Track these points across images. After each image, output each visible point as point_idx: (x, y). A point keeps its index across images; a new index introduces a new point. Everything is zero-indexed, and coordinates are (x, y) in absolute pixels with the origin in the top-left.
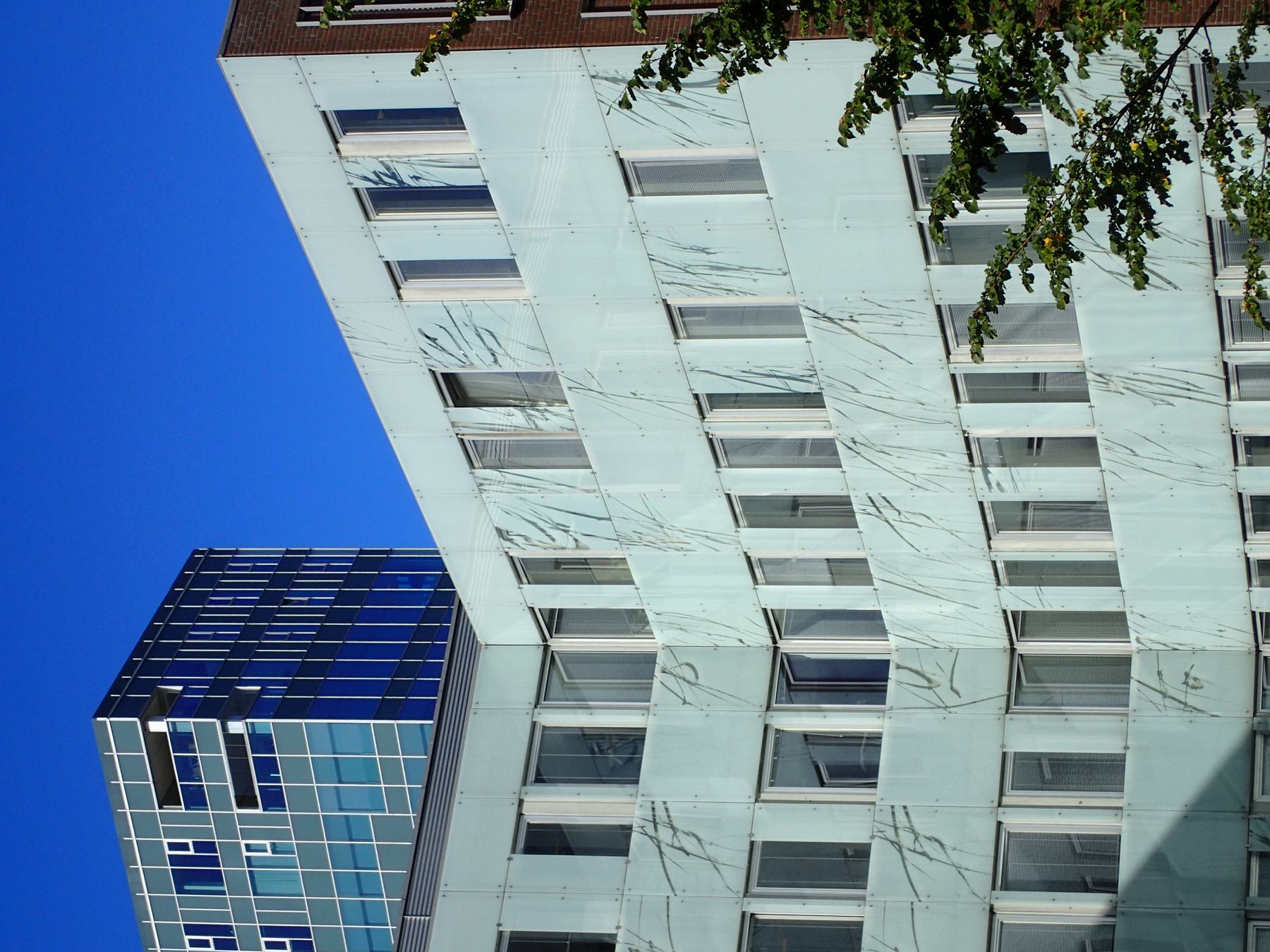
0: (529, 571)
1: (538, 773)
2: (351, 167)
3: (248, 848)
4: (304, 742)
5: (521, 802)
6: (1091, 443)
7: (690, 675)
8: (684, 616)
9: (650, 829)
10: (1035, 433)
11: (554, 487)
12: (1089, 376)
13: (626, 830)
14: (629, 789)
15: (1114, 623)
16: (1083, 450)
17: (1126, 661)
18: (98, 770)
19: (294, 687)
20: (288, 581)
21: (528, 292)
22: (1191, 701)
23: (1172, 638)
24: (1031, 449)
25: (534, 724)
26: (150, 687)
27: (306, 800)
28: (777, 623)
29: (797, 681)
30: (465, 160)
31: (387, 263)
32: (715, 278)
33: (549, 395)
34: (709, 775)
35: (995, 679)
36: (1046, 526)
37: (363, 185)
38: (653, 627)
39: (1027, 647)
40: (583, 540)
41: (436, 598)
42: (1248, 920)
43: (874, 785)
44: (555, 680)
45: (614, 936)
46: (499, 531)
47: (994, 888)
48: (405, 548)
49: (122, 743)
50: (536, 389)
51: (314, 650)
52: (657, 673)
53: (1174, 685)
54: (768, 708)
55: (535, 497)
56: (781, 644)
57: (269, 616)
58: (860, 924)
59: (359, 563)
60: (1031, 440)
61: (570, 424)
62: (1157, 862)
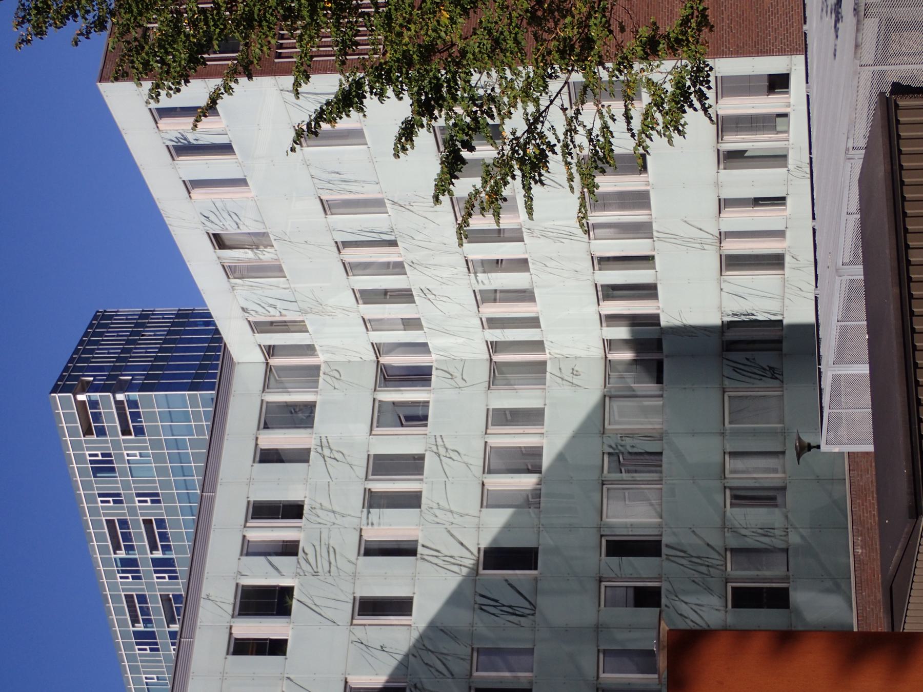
0: (258, 327)
1: (265, 423)
2: (164, 135)
3: (128, 455)
4: (153, 403)
5: (257, 439)
6: (525, 261)
7: (337, 376)
8: (333, 347)
9: (319, 449)
10: (500, 257)
11: (269, 286)
12: (524, 230)
13: (308, 451)
14: (309, 430)
15: (539, 346)
16: (522, 265)
17: (544, 363)
18: (53, 419)
19: (148, 377)
20: (143, 325)
21: (253, 194)
22: (575, 381)
23: (565, 352)
24: (497, 265)
25: (262, 401)
26: (77, 378)
27: (155, 431)
28: (378, 349)
29: (389, 377)
30: (220, 131)
31: (184, 181)
32: (344, 186)
33: (265, 243)
34: (346, 424)
35: (482, 373)
36: (506, 303)
37: (170, 144)
38: (319, 352)
39: (498, 358)
40: (284, 312)
41: (213, 340)
42: (603, 484)
43: (426, 425)
44: (272, 379)
45: (303, 501)
46: (243, 309)
47: (484, 473)
48: (199, 309)
49: (65, 407)
50: (258, 241)
51: (157, 359)
52: (321, 374)
53: (567, 375)
54: (375, 390)
55: (260, 292)
56: (380, 359)
57: (134, 342)
58: (421, 492)
59: (178, 316)
60: (498, 260)
61: (275, 257)
62: (561, 457)
